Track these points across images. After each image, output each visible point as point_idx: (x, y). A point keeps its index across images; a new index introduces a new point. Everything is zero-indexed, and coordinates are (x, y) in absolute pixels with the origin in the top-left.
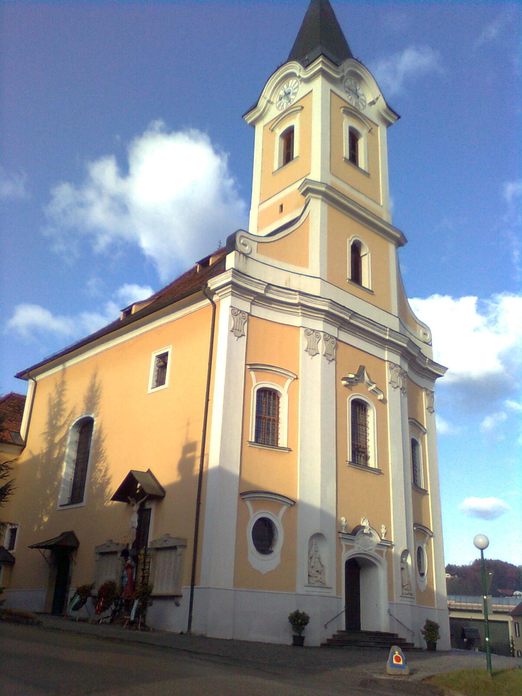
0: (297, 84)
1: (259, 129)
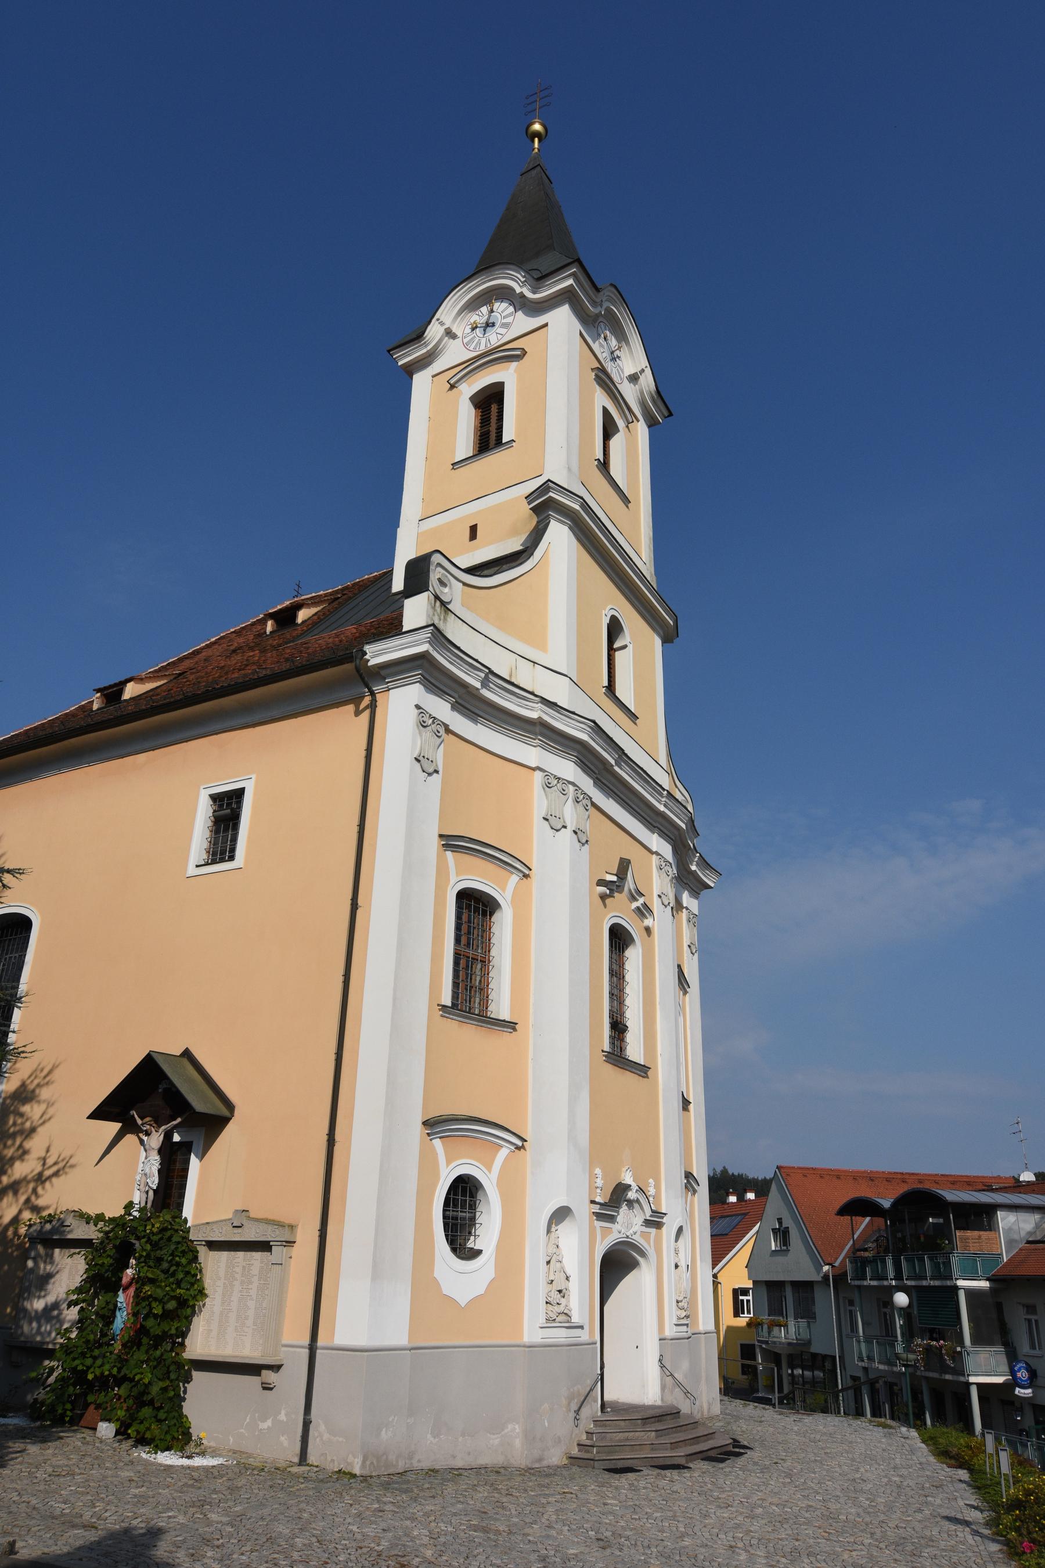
1: (421, 382)
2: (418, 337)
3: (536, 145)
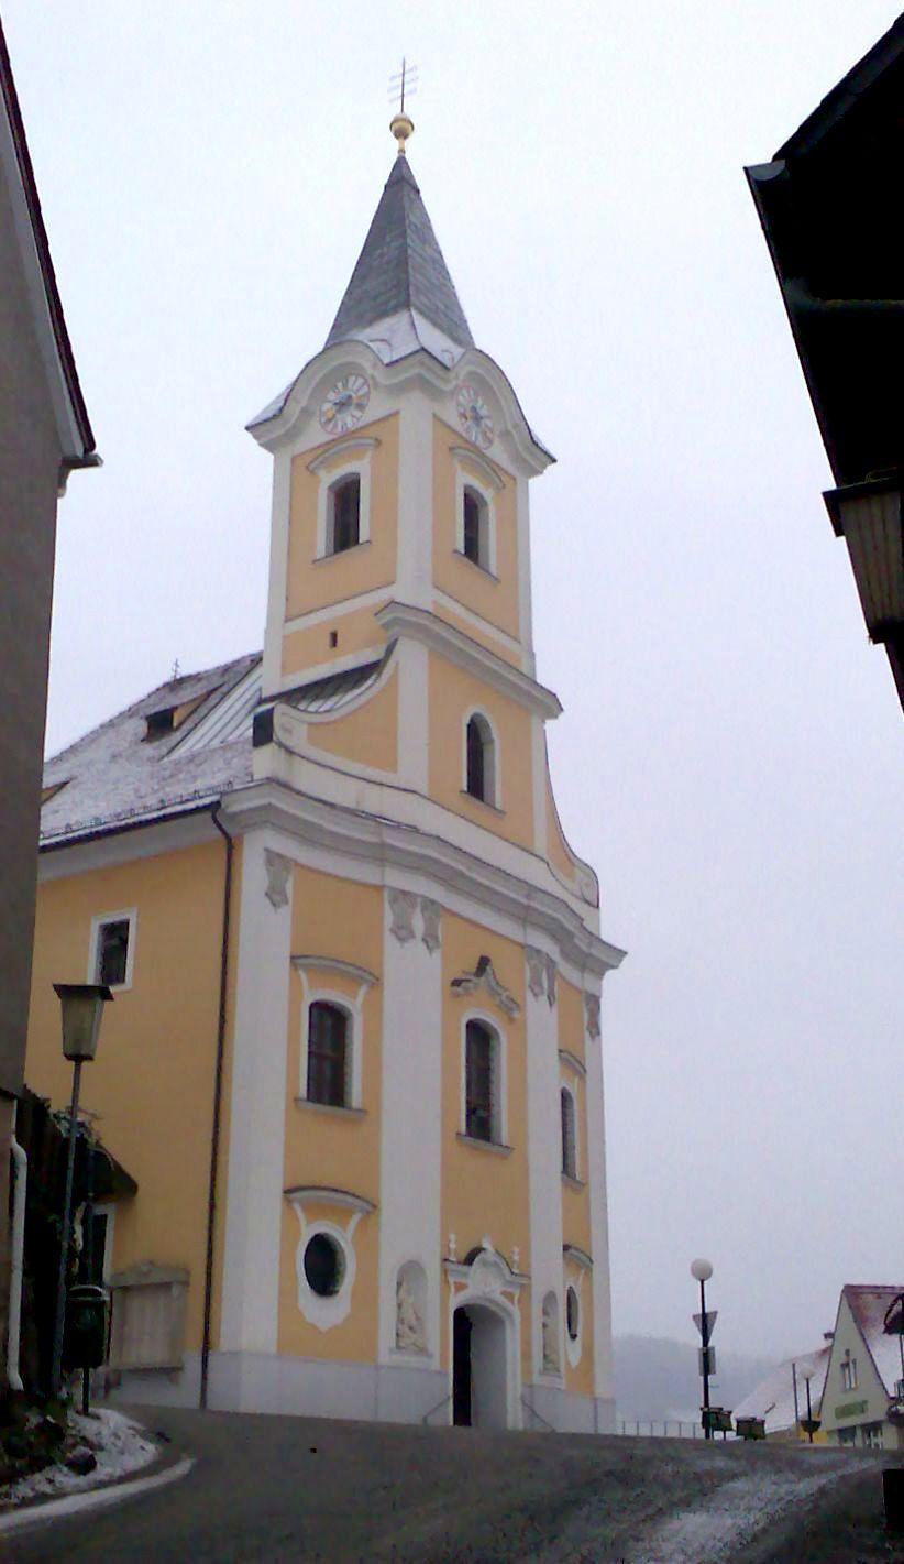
0: (366, 389)
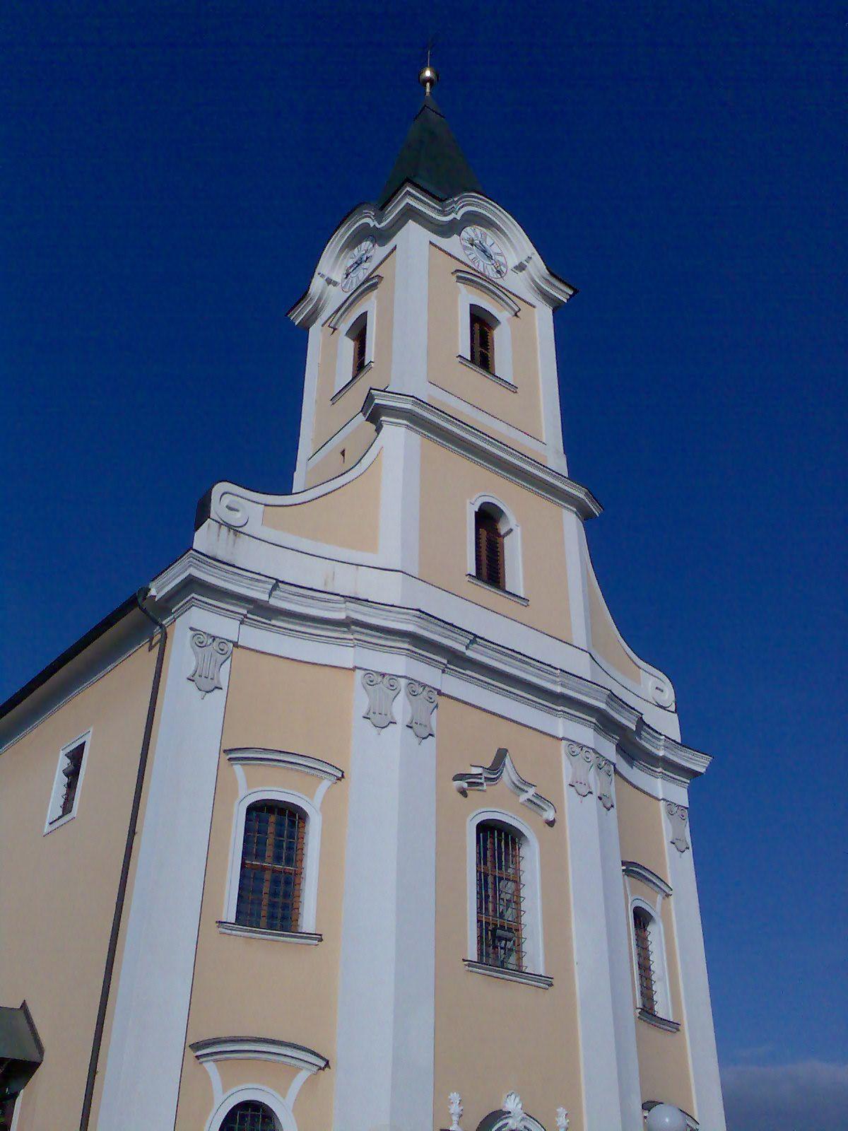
2: (304, 294)
3: (428, 90)
